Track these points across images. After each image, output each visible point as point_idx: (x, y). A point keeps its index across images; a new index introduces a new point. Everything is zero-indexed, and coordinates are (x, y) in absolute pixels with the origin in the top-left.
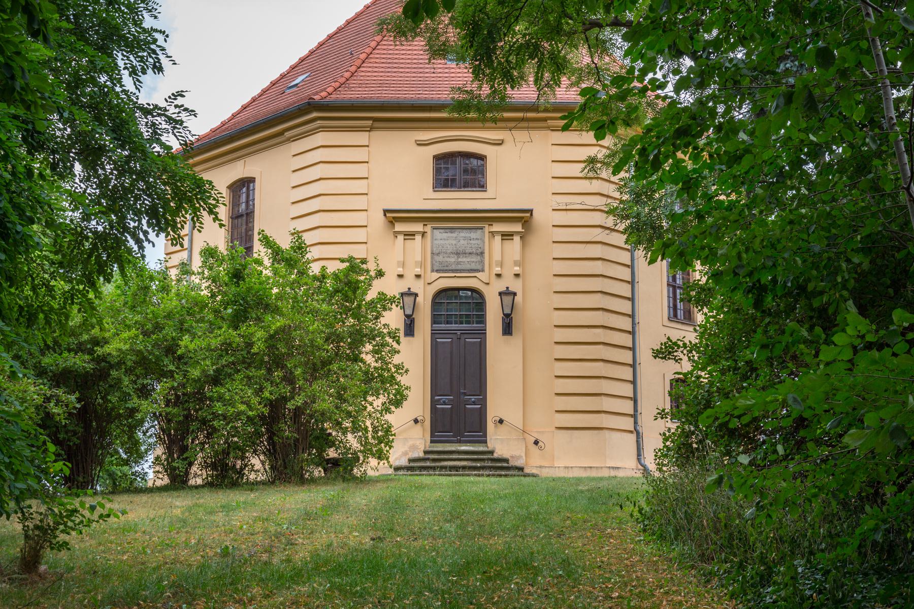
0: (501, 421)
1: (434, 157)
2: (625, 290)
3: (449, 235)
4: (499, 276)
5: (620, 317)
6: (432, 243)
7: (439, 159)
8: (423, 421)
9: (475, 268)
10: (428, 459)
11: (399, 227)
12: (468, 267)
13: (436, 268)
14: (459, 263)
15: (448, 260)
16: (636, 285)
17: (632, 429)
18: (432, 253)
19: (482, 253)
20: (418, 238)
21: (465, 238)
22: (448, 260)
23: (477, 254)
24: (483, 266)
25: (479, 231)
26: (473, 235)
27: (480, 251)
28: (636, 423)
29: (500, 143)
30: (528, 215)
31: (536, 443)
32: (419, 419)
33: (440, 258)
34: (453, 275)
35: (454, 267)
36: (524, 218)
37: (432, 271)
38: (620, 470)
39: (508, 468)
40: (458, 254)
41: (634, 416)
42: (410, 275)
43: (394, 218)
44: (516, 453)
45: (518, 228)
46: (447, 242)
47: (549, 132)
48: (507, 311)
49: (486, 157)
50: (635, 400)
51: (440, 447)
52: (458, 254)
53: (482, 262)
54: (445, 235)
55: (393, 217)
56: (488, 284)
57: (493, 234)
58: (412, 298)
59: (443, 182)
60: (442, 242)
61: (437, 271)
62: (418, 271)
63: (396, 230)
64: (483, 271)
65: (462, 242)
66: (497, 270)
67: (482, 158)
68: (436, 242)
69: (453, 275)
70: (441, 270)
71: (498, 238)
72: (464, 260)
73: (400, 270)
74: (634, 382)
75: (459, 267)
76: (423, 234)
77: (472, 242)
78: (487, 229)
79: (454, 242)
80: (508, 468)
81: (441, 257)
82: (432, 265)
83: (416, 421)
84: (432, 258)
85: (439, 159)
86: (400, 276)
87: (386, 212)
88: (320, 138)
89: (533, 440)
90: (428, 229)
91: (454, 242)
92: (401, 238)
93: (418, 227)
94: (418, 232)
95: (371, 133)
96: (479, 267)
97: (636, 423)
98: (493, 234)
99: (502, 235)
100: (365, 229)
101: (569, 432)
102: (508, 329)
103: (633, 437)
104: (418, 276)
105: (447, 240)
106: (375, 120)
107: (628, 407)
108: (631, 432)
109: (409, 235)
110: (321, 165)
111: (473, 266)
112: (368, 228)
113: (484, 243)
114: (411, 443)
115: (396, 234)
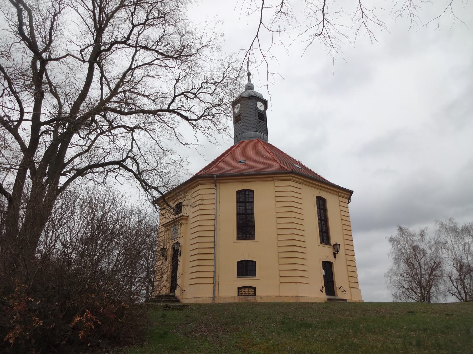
7: (238, 192)
85: (238, 192)
88: (200, 187)
106: (305, 181)
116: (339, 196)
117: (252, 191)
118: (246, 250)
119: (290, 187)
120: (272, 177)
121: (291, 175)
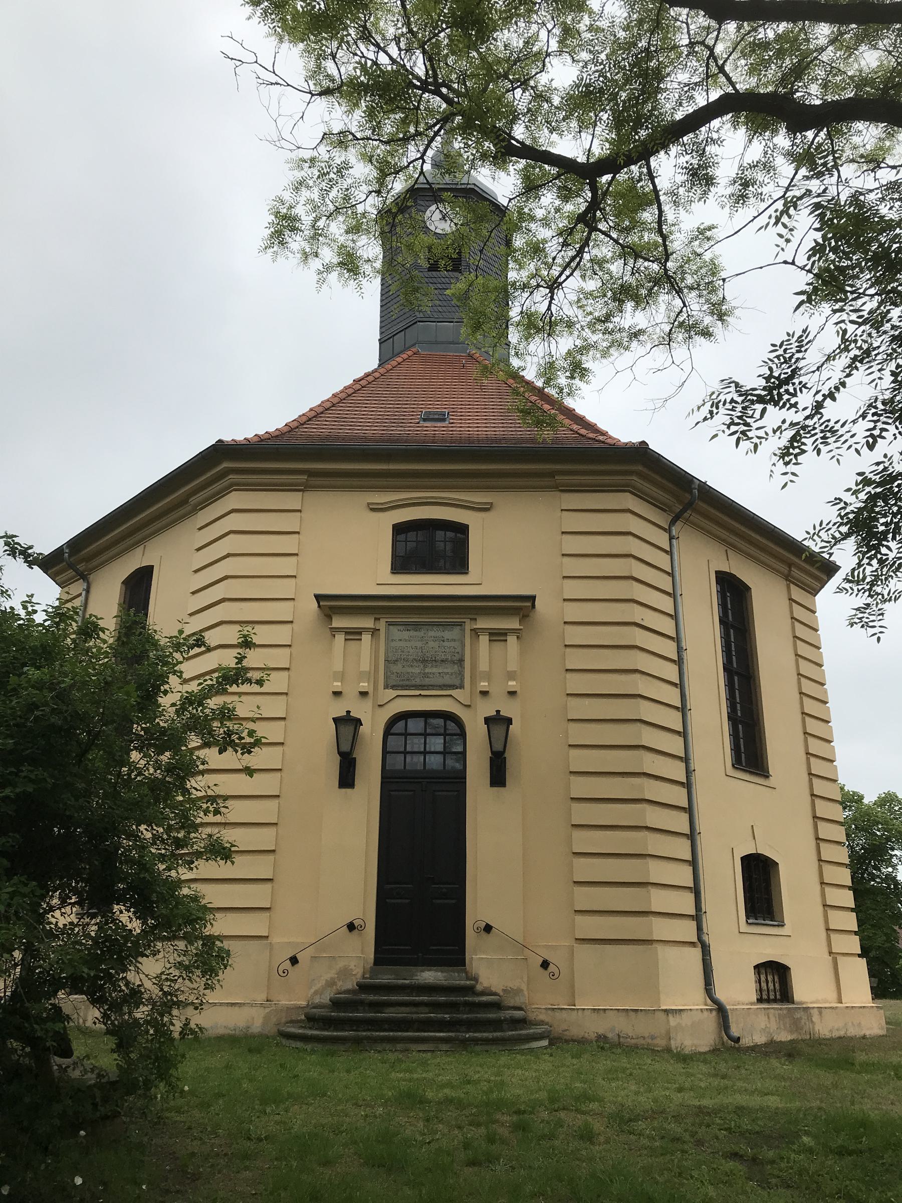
0: (488, 928)
1: (394, 526)
2: (673, 720)
3: (412, 633)
4: (484, 693)
5: (666, 811)
6: (387, 644)
7: (399, 529)
8: (362, 928)
9: (450, 682)
10: (362, 1002)
11: (339, 622)
12: (440, 681)
13: (392, 683)
14: (426, 675)
15: (410, 670)
16: (689, 713)
17: (695, 939)
18: (387, 661)
19: (461, 661)
20: (366, 638)
21: (435, 639)
22: (410, 670)
23: (453, 662)
24: (462, 680)
25: (457, 630)
26: (447, 634)
27: (457, 657)
28: (699, 929)
29: (486, 508)
30: (529, 604)
31: (545, 965)
32: (356, 923)
33: (398, 668)
34: (417, 692)
35: (418, 681)
36: (521, 606)
37: (386, 687)
38: (684, 1015)
39: (497, 1024)
40: (424, 661)
41: (698, 917)
42: (351, 692)
43: (331, 608)
44: (513, 984)
45: (513, 623)
46: (408, 644)
47: (558, 493)
48: (498, 747)
49: (467, 527)
50: (696, 891)
51: (386, 979)
52: (424, 661)
53: (461, 674)
54: (406, 635)
55: (331, 605)
56: (468, 706)
57: (476, 632)
58: (352, 728)
59: (402, 563)
60: (402, 644)
61: (394, 687)
62: (364, 686)
63: (334, 625)
64: (461, 687)
65: (431, 644)
66: (484, 685)
67: (462, 530)
68: (393, 644)
69: (417, 692)
70: (398, 683)
71: (484, 639)
72: (434, 670)
73: (337, 685)
74: (694, 863)
75: (427, 681)
76: (374, 632)
77: (446, 644)
78: (469, 626)
79: (419, 644)
80: (497, 1024)
81: (400, 665)
82: (387, 677)
83: (351, 927)
84: (386, 667)
85: (399, 529)
86: (337, 694)
87: (319, 598)
88: (234, 500)
89: (541, 960)
90: (382, 625)
91: (419, 644)
92: (340, 638)
93: (367, 622)
94: (366, 630)
95: (306, 494)
96: (457, 683)
97: (699, 929)
98: (476, 632)
99: (491, 634)
100: (289, 626)
101: (656, 529)
102: (498, 775)
103: (696, 953)
104: (364, 694)
105: (408, 641)
106: (311, 473)
107: (685, 876)
108: (693, 944)
109: (354, 634)
110: (231, 536)
111: (447, 680)
112: (294, 625)
113: (463, 646)
114: (341, 964)
115: (334, 631)
116: (788, 578)
117: (462, 530)
118: (767, 946)
119: (635, 522)
120: (552, 474)
121: (226, 465)
